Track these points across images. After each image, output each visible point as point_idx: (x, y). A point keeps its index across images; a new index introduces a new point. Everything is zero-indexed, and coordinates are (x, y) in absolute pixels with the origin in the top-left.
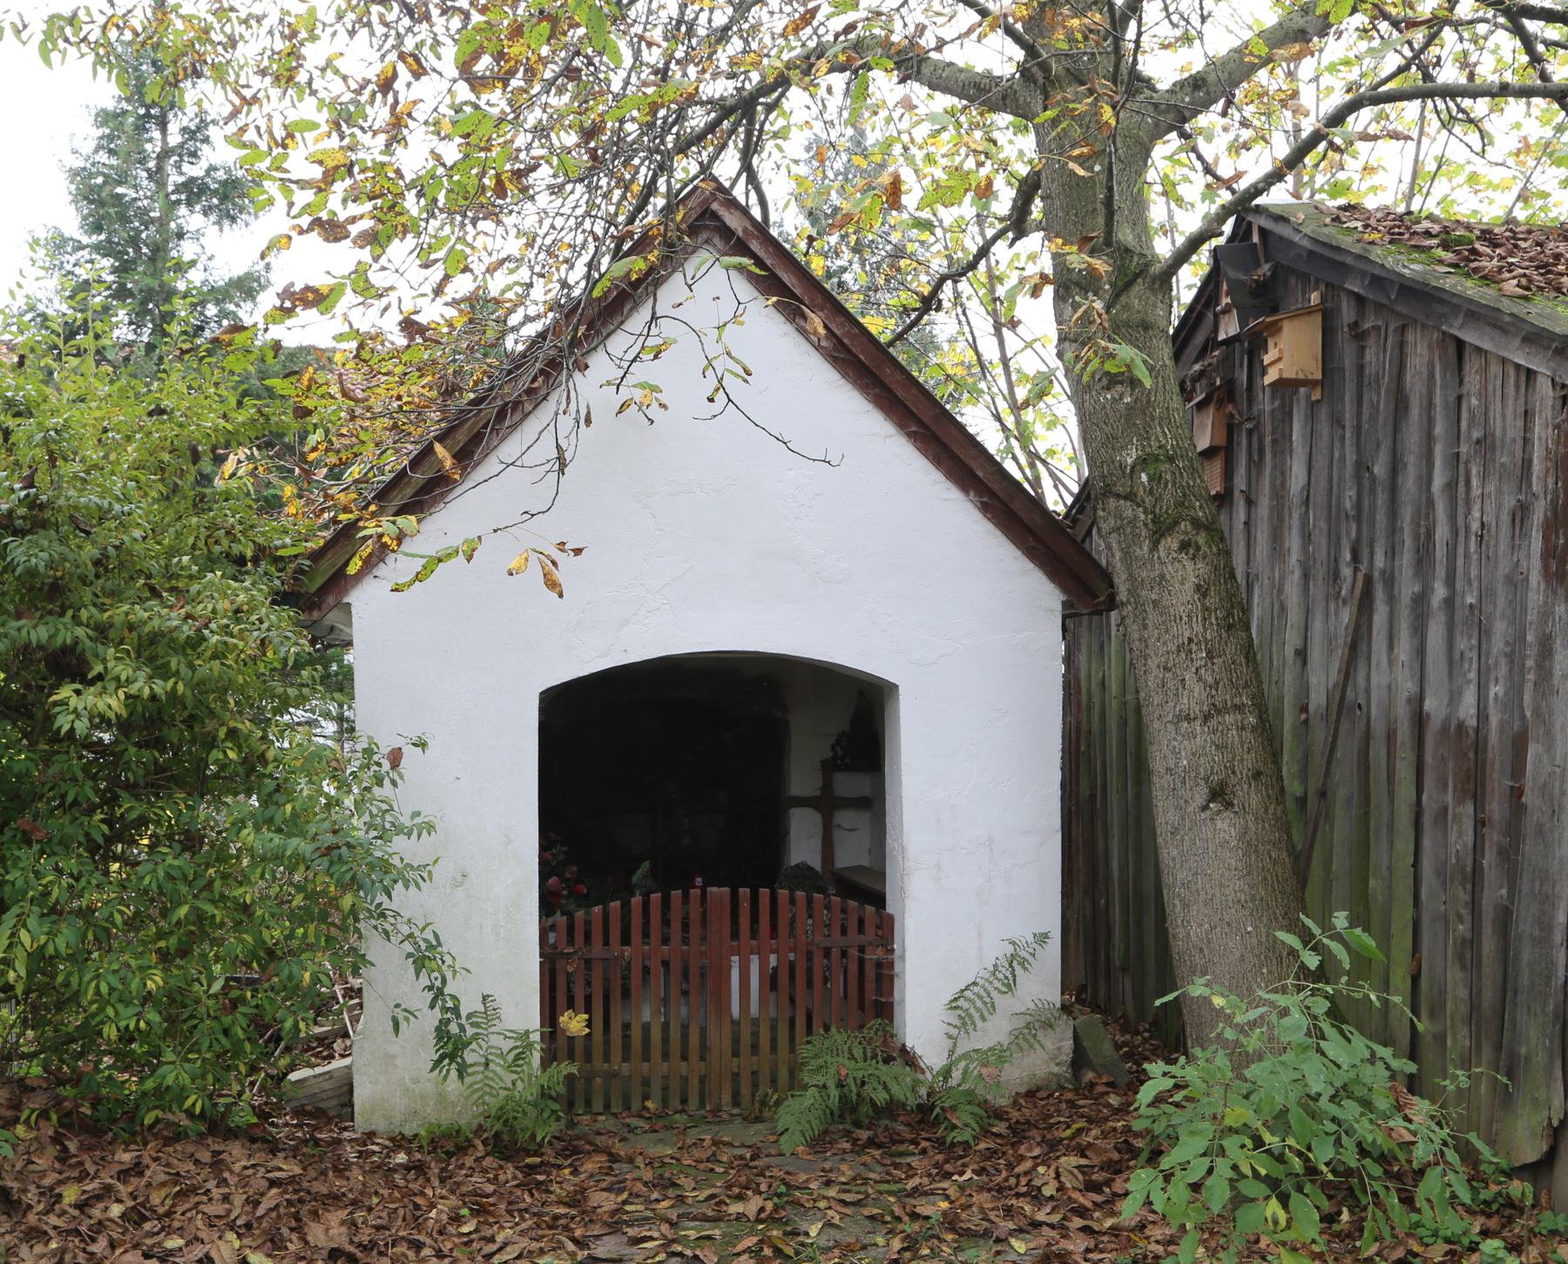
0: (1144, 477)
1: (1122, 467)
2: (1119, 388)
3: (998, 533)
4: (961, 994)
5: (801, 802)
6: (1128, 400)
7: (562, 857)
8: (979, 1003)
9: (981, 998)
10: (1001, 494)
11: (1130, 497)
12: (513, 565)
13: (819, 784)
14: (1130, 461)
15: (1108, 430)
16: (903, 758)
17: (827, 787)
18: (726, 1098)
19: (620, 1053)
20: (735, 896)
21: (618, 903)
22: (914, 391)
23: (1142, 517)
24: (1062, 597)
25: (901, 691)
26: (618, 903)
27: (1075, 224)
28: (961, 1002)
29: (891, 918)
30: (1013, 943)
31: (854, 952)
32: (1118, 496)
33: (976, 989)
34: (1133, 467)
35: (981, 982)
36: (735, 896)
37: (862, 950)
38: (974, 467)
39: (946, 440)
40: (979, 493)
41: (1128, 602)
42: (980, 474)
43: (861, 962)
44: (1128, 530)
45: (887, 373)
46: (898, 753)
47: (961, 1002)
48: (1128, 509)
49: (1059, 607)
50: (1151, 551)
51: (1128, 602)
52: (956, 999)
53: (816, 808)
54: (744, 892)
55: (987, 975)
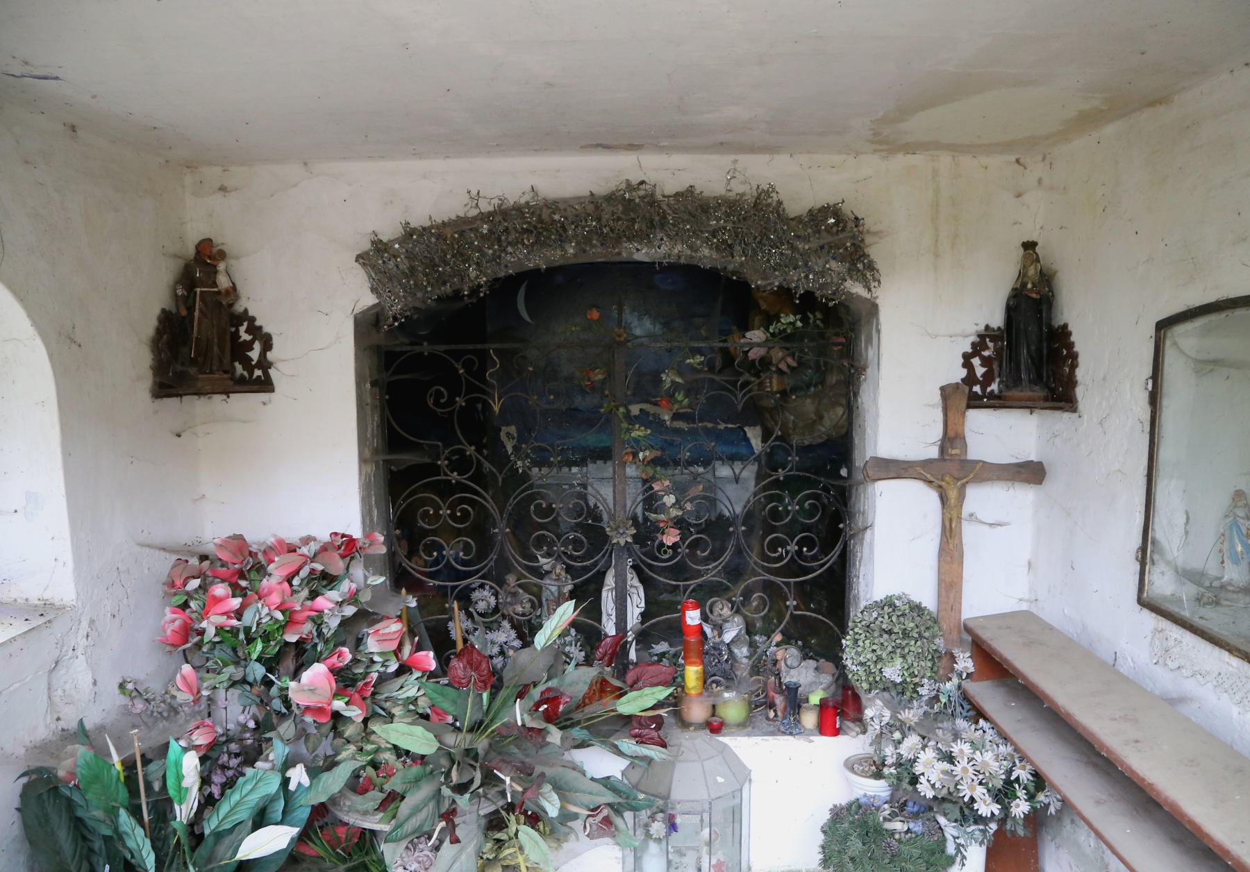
13: (937, 432)
17: (952, 439)
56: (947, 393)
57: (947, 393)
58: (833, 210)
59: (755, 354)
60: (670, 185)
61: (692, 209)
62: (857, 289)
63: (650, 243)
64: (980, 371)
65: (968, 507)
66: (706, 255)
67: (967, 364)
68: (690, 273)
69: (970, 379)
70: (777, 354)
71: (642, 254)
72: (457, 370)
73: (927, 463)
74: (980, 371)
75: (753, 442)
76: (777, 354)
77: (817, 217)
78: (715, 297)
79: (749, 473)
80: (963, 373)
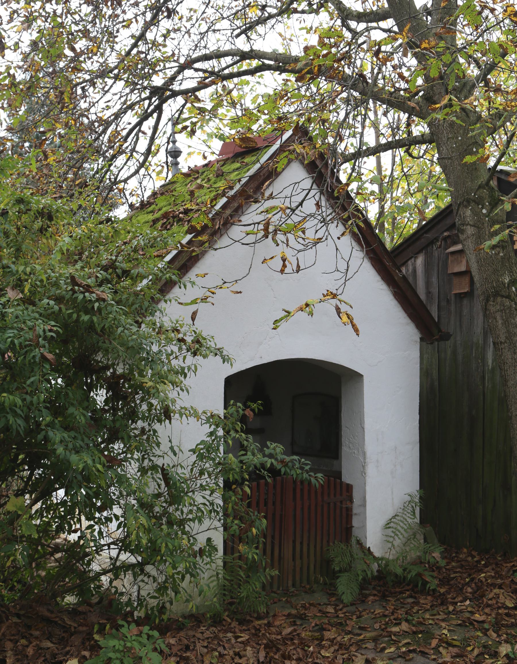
0: (514, 289)
1: (504, 284)
2: (498, 249)
3: (399, 305)
4: (390, 521)
6: (502, 254)
8: (401, 524)
9: (401, 521)
11: (508, 297)
12: (303, 315)
14: (506, 281)
15: (494, 267)
16: (366, 410)
18: (290, 583)
23: (514, 306)
25: (365, 378)
27: (467, 173)
28: (392, 525)
29: (349, 488)
30: (409, 495)
31: (338, 504)
32: (503, 296)
33: (398, 518)
34: (508, 284)
35: (400, 514)
37: (341, 502)
40: (393, 288)
41: (505, 342)
43: (341, 508)
44: (508, 311)
47: (392, 525)
48: (507, 302)
49: (419, 340)
51: (505, 342)
52: (388, 524)
55: (401, 511)
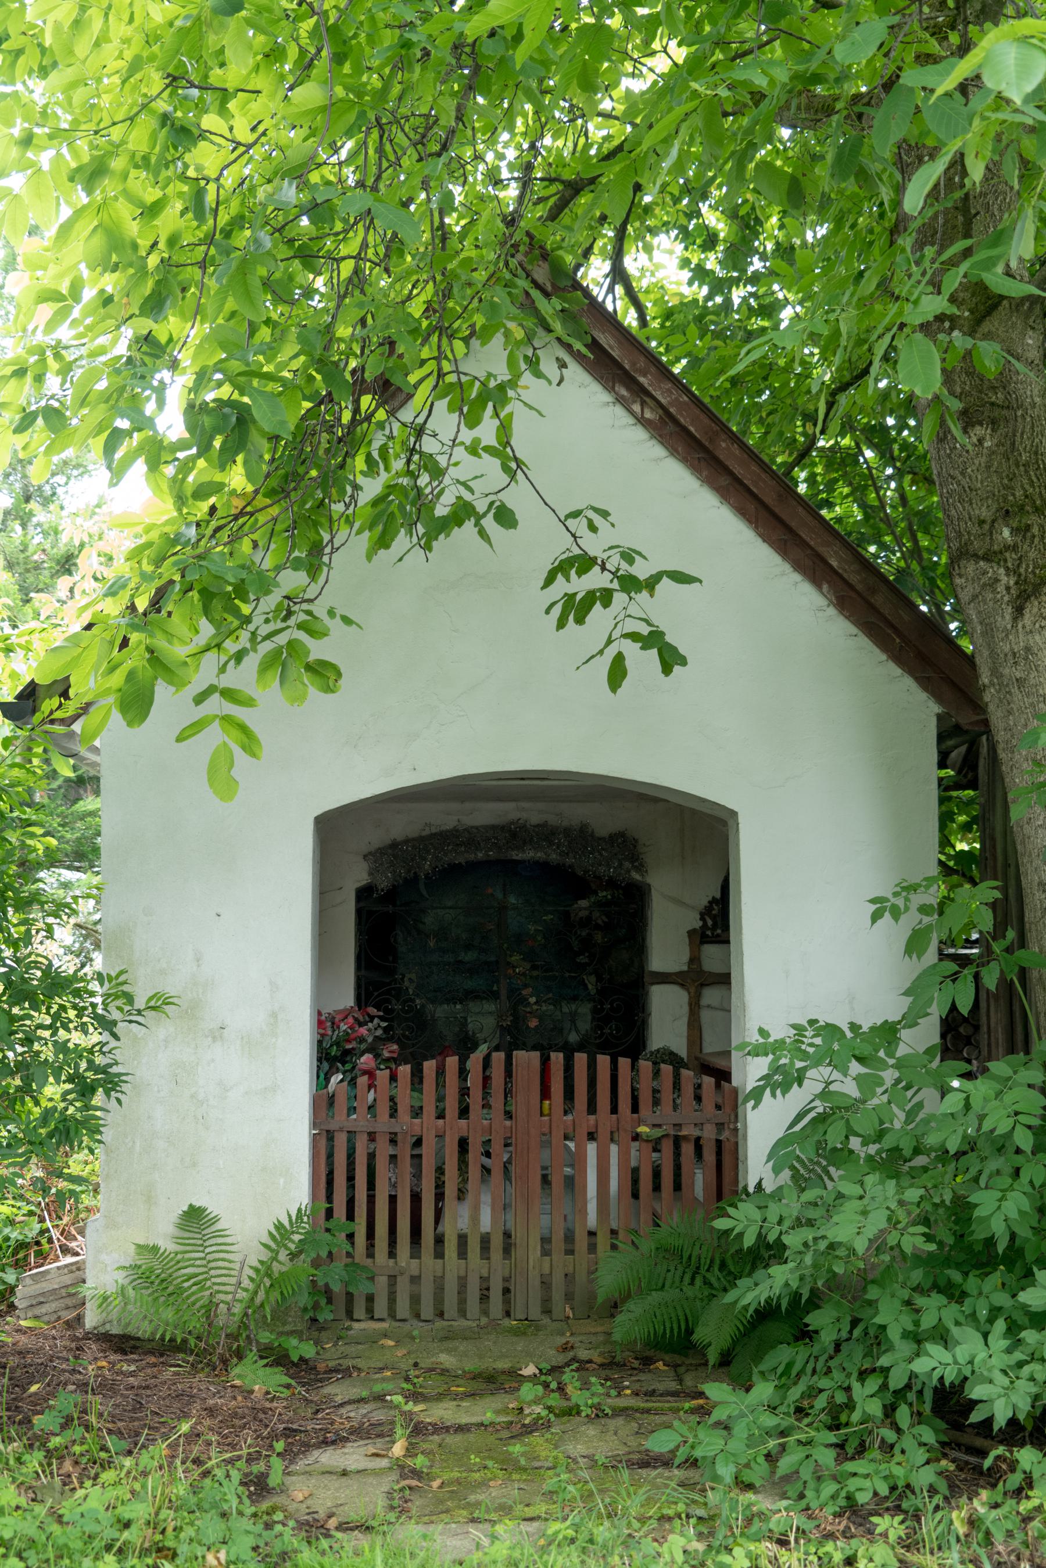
5: (664, 978)
7: (379, 1032)
10: (859, 587)
13: (686, 957)
17: (695, 959)
19: (447, 1287)
20: (545, 1062)
21: (408, 1067)
22: (754, 468)
24: (936, 708)
26: (408, 1067)
32: (976, 557)
36: (545, 1062)
38: (826, 555)
39: (793, 524)
42: (834, 564)
45: (723, 448)
46: (739, 892)
50: (1015, 619)
53: (682, 985)
54: (557, 1058)
56: (691, 933)
57: (691, 933)
58: (622, 834)
59: (584, 914)
60: (535, 819)
61: (546, 834)
62: (636, 876)
63: (524, 851)
64: (710, 923)
65: (704, 1001)
66: (554, 857)
67: (702, 919)
68: (544, 867)
69: (705, 925)
70: (596, 914)
71: (516, 855)
72: (917, 607)
73: (680, 974)
74: (710, 923)
75: (590, 987)
76: (596, 914)
77: (613, 838)
78: (559, 881)
79: (585, 1009)
80: (701, 923)
